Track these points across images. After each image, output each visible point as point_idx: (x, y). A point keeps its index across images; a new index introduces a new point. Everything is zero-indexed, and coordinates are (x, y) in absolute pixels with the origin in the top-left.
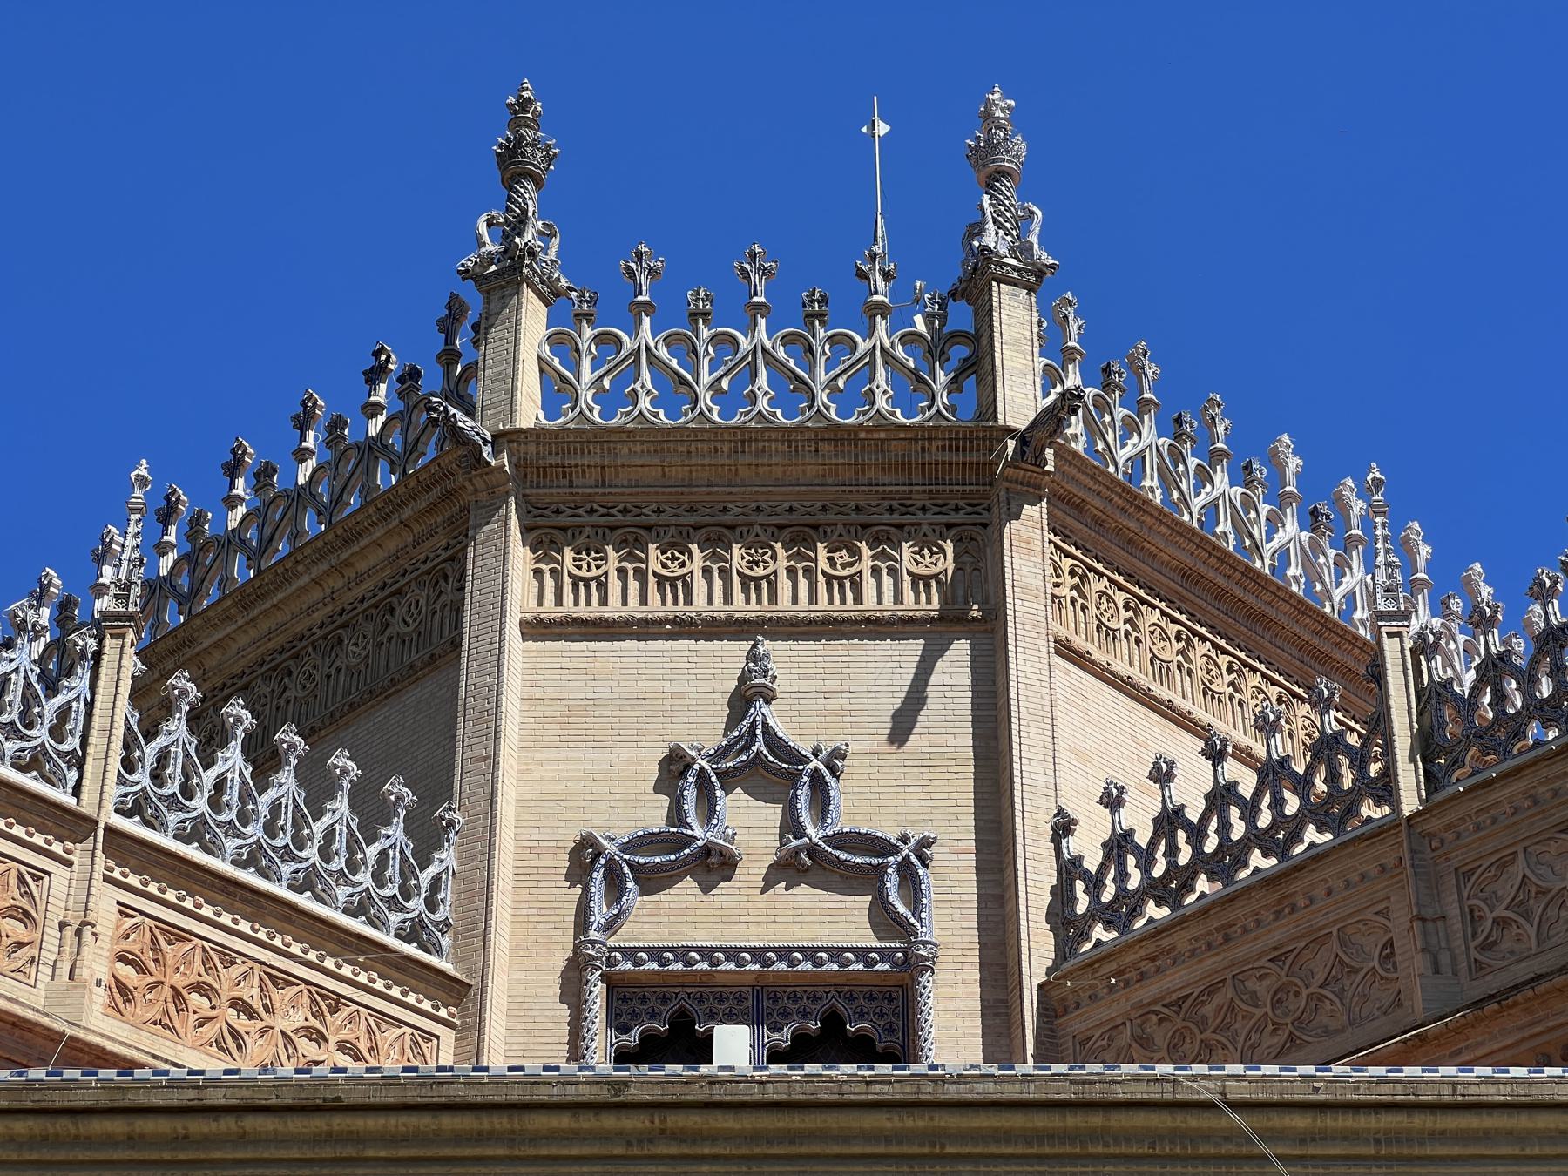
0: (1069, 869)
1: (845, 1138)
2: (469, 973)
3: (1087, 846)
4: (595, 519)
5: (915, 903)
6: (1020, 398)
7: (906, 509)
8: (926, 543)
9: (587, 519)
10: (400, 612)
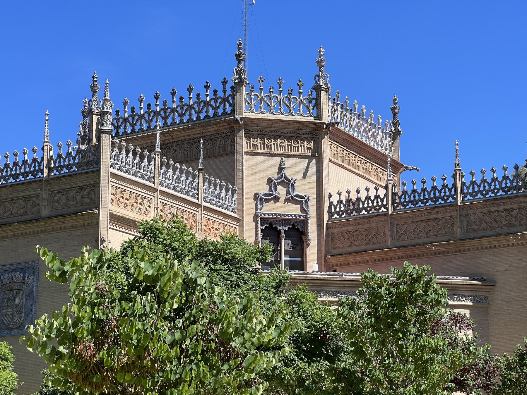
0: (331, 203)
1: (333, 284)
2: (240, 217)
3: (335, 201)
4: (256, 133)
5: (308, 209)
6: (326, 118)
7: (306, 134)
8: (309, 141)
9: (254, 133)
10: (218, 142)
